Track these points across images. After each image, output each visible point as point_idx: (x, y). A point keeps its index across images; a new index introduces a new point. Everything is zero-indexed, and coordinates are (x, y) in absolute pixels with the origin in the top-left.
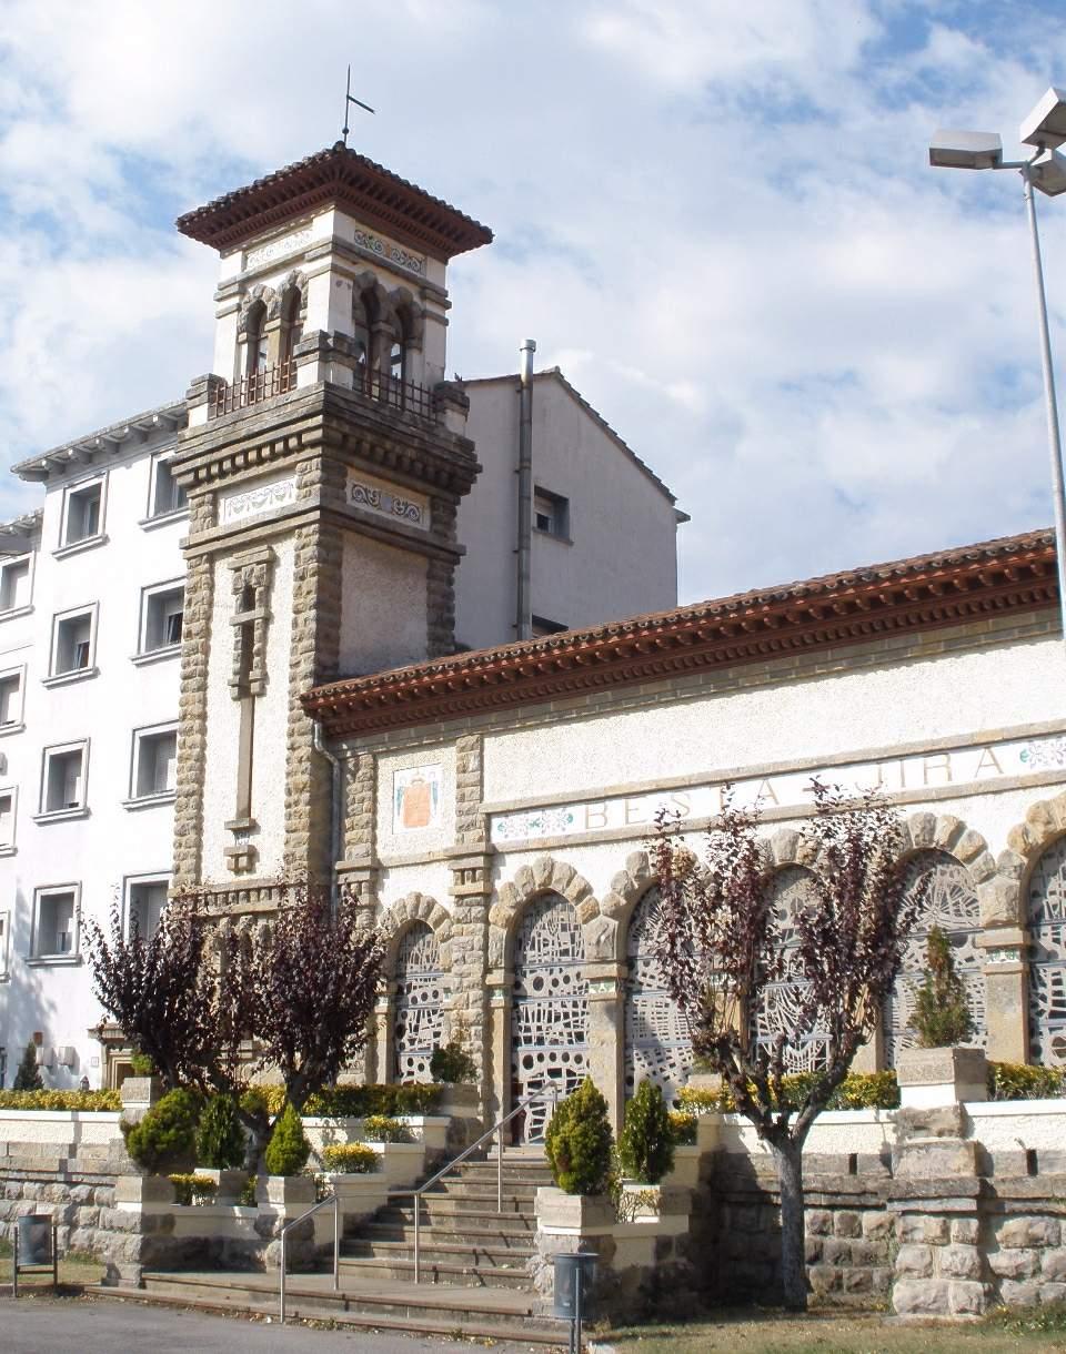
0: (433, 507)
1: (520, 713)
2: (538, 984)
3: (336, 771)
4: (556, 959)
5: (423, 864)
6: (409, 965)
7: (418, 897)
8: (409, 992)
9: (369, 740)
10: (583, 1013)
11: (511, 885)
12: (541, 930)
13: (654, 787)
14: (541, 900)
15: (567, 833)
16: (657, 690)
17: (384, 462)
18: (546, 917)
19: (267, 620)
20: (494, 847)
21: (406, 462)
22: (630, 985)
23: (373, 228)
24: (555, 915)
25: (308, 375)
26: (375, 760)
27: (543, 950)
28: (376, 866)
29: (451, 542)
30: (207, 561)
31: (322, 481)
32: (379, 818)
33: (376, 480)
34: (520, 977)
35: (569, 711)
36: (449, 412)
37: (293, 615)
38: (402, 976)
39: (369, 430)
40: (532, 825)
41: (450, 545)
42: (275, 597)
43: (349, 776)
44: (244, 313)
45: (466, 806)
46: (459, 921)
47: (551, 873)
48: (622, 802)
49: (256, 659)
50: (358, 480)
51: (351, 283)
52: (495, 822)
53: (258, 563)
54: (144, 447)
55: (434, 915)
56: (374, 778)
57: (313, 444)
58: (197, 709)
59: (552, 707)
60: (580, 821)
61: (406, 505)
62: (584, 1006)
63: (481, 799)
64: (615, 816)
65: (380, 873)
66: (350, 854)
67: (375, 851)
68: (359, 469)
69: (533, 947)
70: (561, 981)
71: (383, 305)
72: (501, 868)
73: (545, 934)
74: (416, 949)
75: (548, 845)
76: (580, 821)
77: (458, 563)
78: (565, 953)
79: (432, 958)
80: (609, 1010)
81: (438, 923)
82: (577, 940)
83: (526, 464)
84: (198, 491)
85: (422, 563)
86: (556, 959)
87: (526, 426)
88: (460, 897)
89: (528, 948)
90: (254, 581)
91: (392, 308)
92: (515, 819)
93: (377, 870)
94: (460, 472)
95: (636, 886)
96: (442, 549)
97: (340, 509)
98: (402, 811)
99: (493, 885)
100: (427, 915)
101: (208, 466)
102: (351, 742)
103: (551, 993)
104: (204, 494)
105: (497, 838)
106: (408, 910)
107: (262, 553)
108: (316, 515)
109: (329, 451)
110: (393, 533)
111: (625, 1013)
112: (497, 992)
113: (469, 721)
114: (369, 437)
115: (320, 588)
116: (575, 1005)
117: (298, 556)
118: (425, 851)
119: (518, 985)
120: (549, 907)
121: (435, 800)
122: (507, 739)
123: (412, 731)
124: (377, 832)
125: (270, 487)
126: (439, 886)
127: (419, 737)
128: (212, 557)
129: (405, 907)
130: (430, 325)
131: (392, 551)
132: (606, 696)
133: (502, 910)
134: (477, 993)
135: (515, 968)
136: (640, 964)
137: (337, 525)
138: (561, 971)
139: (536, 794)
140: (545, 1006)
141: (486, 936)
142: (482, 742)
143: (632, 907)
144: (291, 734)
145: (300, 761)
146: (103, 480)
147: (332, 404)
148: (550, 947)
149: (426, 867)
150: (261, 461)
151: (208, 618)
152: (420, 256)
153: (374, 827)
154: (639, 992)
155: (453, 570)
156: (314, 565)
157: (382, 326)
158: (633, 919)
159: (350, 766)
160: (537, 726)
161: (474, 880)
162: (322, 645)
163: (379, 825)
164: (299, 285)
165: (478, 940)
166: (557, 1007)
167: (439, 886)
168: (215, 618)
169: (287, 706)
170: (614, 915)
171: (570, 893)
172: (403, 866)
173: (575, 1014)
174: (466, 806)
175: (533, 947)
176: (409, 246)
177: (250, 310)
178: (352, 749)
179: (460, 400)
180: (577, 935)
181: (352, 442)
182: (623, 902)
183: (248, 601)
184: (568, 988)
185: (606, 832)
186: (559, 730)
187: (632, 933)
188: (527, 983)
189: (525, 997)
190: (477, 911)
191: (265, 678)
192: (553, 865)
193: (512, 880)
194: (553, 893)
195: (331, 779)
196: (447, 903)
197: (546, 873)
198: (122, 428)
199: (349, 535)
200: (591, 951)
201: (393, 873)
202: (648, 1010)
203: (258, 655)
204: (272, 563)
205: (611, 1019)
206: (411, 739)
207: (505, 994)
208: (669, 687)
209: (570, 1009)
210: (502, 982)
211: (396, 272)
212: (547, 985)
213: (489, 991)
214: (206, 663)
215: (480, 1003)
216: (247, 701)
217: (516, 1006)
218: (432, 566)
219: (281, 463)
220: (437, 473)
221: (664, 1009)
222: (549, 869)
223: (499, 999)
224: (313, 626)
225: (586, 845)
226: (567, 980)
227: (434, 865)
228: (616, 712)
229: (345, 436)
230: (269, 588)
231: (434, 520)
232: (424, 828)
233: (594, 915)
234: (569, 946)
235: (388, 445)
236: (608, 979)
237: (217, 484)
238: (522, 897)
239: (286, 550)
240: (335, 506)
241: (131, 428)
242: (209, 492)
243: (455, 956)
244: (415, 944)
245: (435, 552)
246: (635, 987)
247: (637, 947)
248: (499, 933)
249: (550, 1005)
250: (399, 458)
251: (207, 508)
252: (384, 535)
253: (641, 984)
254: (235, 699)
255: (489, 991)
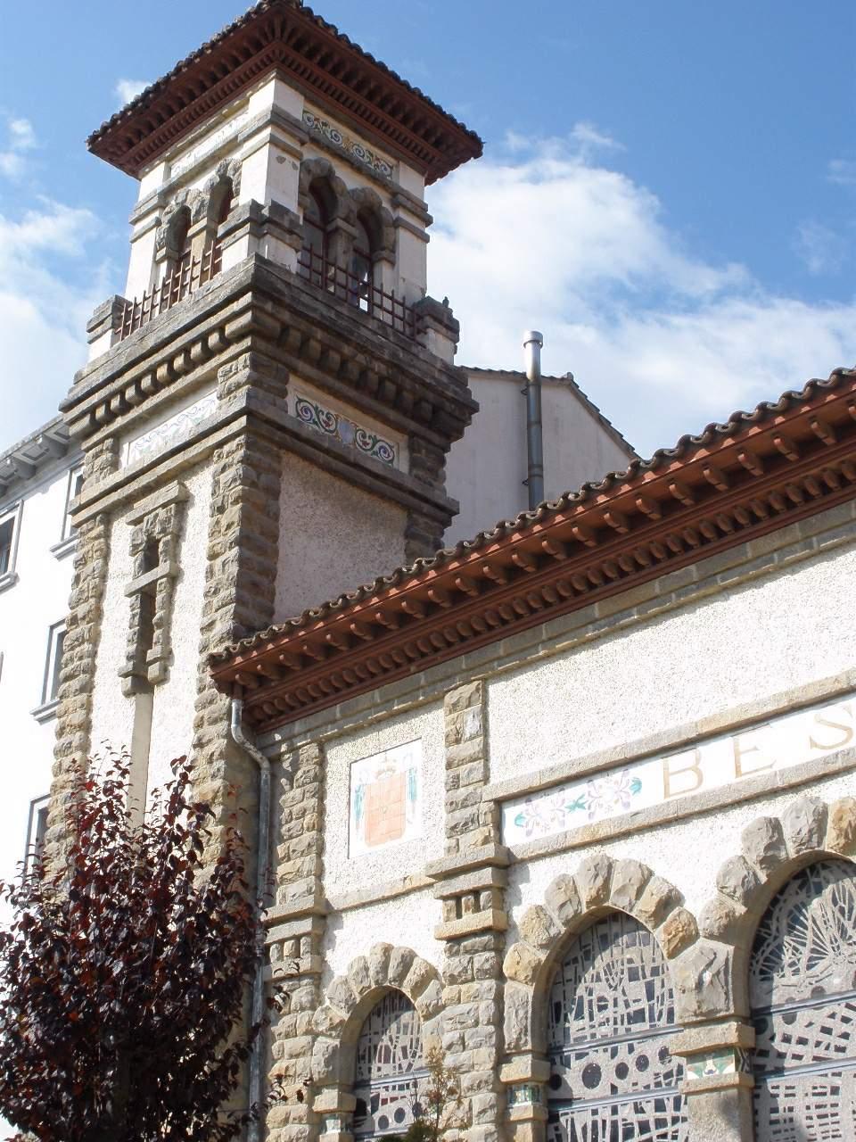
0: (412, 449)
1: (545, 631)
2: (592, 1076)
3: (265, 775)
4: (621, 1030)
5: (395, 897)
6: (374, 1067)
7: (387, 950)
8: (374, 1109)
9: (312, 721)
10: (675, 1120)
11: (539, 909)
12: (593, 984)
13: (784, 703)
14: (594, 930)
15: (633, 809)
16: (777, 544)
17: (341, 373)
18: (600, 963)
19: (174, 578)
20: (509, 852)
21: (373, 378)
22: (761, 1061)
23: (328, 113)
24: (621, 953)
25: (237, 255)
26: (322, 751)
27: (599, 1017)
28: (323, 910)
29: (437, 492)
30: (101, 522)
31: (250, 380)
32: (328, 836)
33: (330, 399)
34: (558, 1068)
35: (625, 611)
36: (431, 333)
37: (208, 563)
38: (363, 1084)
39: (319, 325)
40: (572, 808)
41: (435, 495)
42: (185, 548)
43: (283, 781)
44: (165, 226)
45: (462, 793)
46: (453, 980)
47: (607, 881)
48: (725, 743)
49: (157, 633)
50: (306, 394)
51: (298, 164)
52: (510, 812)
53: (164, 506)
54: (63, 463)
55: (411, 978)
56: (321, 779)
57: (239, 336)
58: (77, 717)
59: (596, 610)
60: (653, 787)
61: (376, 441)
62: (677, 1107)
63: (486, 780)
64: (716, 768)
65: (329, 921)
66: (284, 896)
67: (321, 889)
68: (307, 379)
69: (579, 1016)
70: (632, 1067)
71: (341, 199)
72: (522, 887)
73: (601, 989)
74: (385, 1038)
75: (602, 833)
76: (653, 787)
77: (448, 523)
78: (638, 1016)
79: (410, 1051)
80: (726, 1108)
81: (419, 987)
82: (658, 992)
83: (536, 471)
84: (95, 438)
85: (399, 516)
86: (621, 1030)
87: (534, 428)
88: (454, 940)
89: (571, 1017)
90: (158, 528)
91: (355, 208)
92: (542, 803)
93: (324, 917)
94: (449, 406)
95: (763, 878)
96: (427, 501)
97: (277, 419)
98: (363, 821)
99: (509, 916)
100: (401, 977)
101: (106, 401)
102: (286, 729)
103: (614, 1089)
104: (101, 441)
105: (515, 838)
106: (371, 973)
107: (171, 491)
108: (243, 421)
109: (262, 345)
110: (356, 465)
111: (755, 1112)
112: (520, 1094)
113: (463, 662)
114: (320, 334)
115: (245, 518)
116: (660, 1106)
117: (217, 483)
118: (398, 876)
119: (556, 1081)
120: (606, 942)
121: (413, 796)
122: (526, 680)
123: (377, 695)
124: (325, 858)
125: (185, 412)
126: (420, 930)
127: (388, 702)
128: (108, 516)
129: (367, 969)
130: (404, 237)
131: (356, 494)
132: (689, 574)
133: (525, 954)
134: (483, 1098)
135: (550, 1053)
136: (777, 1022)
137: (268, 439)
138: (631, 1049)
139: (575, 755)
140: (606, 1114)
141: (499, 999)
142: (486, 691)
143: (756, 918)
144: (199, 725)
145: (210, 761)
146: (16, 513)
147: (263, 282)
148: (609, 1013)
149: (398, 903)
150: (174, 376)
151: (100, 596)
152: (392, 161)
153: (321, 851)
154: (779, 1071)
155: (442, 534)
156: (238, 488)
157: (340, 223)
158: (758, 943)
159: (286, 765)
160: (573, 649)
161: (477, 908)
162: (247, 596)
163: (328, 847)
164: (230, 173)
165: (485, 1008)
166: (627, 1113)
167: (420, 930)
168: (108, 595)
169: (194, 687)
170: (724, 935)
171: (647, 904)
172: (363, 905)
173: (660, 1123)
174: (462, 793)
175: (579, 1016)
176: (375, 145)
177: (170, 221)
178: (289, 739)
179: (446, 321)
180: (657, 984)
181: (295, 337)
182: (740, 909)
183: (150, 562)
184: (646, 1077)
185: (703, 795)
186: (610, 648)
187: (757, 968)
188: (573, 1077)
189: (568, 1102)
190: (483, 959)
191: (167, 657)
192: (610, 867)
193: (542, 902)
194: (617, 916)
195: (257, 790)
196: (432, 954)
197: (600, 881)
198: (35, 439)
199: (290, 459)
200: (684, 1005)
201: (349, 919)
202: (799, 1103)
203: (159, 626)
204: (182, 504)
205: (730, 1122)
206: (376, 706)
207: (535, 1097)
208: (799, 535)
209: (650, 1115)
210: (532, 1116)
211: (358, 168)
212: (608, 1076)
213: (506, 1093)
214: (94, 654)
215: (491, 1115)
216: (143, 697)
217: (554, 1118)
218: (412, 523)
219: (200, 372)
220: (417, 403)
221: (829, 1099)
222: (604, 872)
223: (523, 1106)
224: (234, 569)
225: (666, 824)
226: (642, 1063)
227: (412, 897)
228: (706, 599)
229: (285, 328)
230: (178, 536)
231: (414, 463)
232: (396, 843)
233: (688, 939)
234: (644, 1004)
235: (347, 350)
236: (718, 1051)
237: (120, 421)
238: (559, 928)
239: (201, 486)
240: (270, 413)
241: (46, 438)
242: (107, 437)
243: (447, 1038)
244: (384, 1032)
245: (416, 502)
246: (770, 1063)
247: (770, 992)
248: (521, 993)
249: (615, 1111)
250: (364, 372)
251: (107, 456)
252: (341, 466)
253: (781, 1056)
254: (127, 694)
255: (506, 1093)
